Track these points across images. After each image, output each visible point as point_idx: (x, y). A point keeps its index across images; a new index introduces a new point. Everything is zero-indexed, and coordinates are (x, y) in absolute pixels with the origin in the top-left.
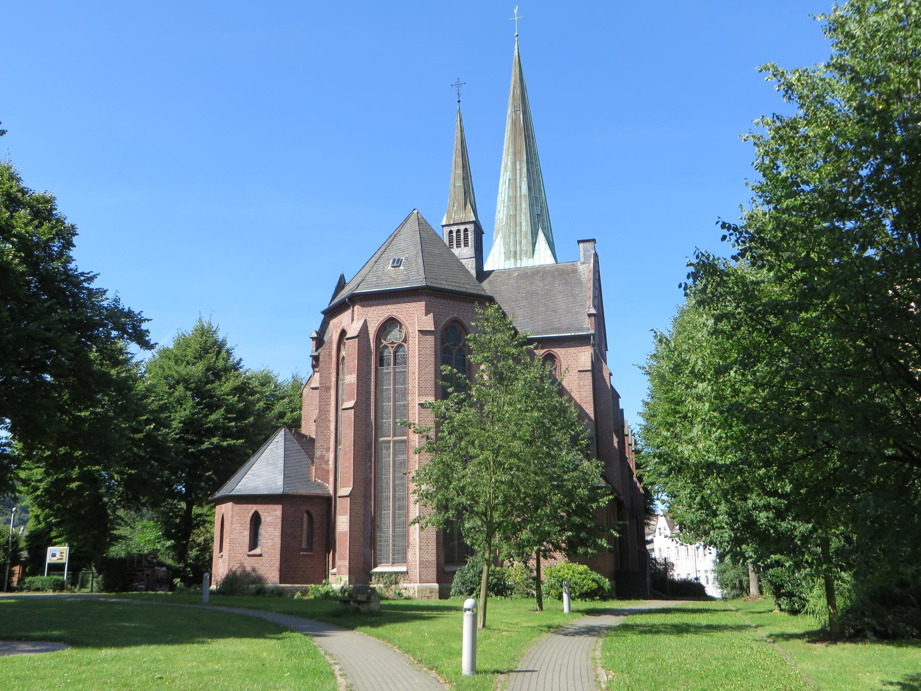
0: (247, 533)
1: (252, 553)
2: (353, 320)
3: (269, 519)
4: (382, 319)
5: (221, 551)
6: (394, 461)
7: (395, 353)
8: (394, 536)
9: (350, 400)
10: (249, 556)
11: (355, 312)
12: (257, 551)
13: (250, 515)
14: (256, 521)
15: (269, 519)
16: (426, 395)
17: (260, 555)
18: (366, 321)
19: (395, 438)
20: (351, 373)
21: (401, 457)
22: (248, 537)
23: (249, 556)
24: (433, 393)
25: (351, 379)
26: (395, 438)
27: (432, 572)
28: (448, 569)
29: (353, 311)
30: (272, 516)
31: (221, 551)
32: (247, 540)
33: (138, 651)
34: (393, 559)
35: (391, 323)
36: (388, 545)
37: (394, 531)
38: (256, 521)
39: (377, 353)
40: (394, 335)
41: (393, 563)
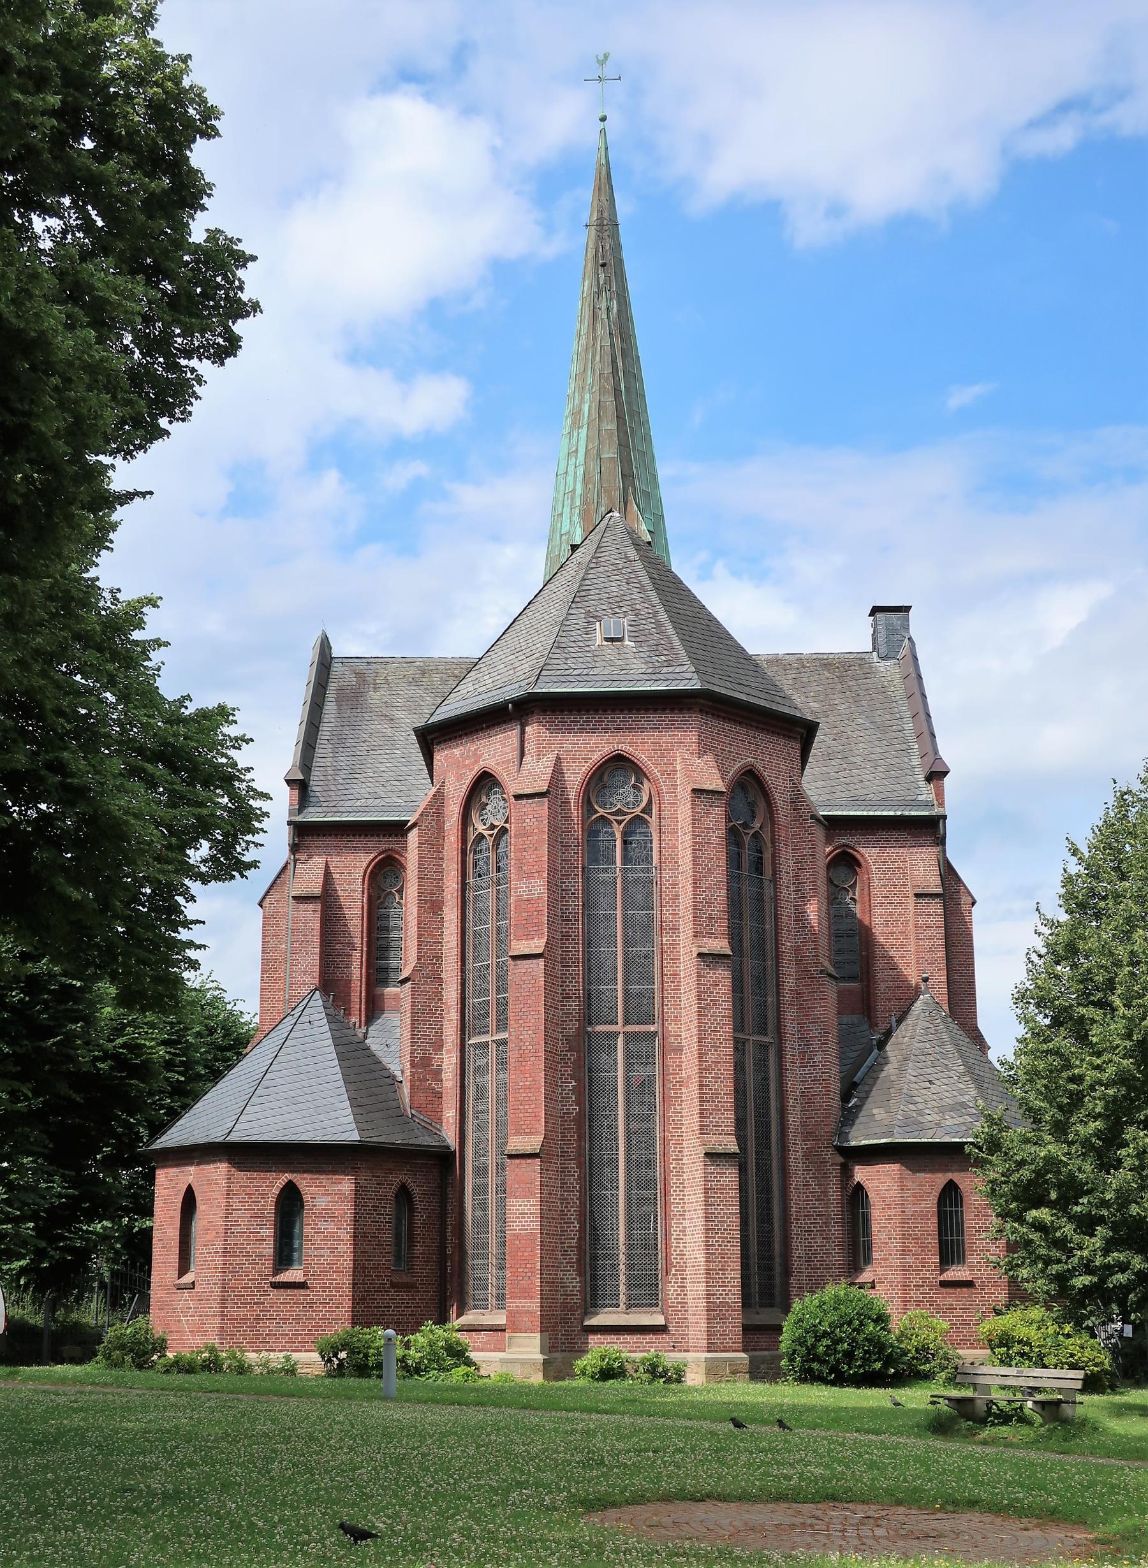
0: (268, 1233)
1: (284, 1277)
2: (522, 754)
3: (322, 1202)
4: (596, 757)
5: (184, 1266)
6: (627, 1079)
7: (625, 834)
8: (630, 1247)
9: (529, 936)
10: (275, 1285)
11: (530, 746)
12: (293, 1275)
13: (276, 1191)
14: (290, 1205)
15: (322, 1202)
16: (711, 935)
17: (302, 1285)
18: (558, 758)
19: (630, 1028)
20: (530, 876)
21: (642, 1072)
22: (271, 1241)
23: (275, 1285)
24: (724, 930)
25: (530, 887)
26: (630, 1028)
27: (733, 1326)
28: (765, 1317)
29: (523, 732)
30: (330, 1199)
31: (184, 1266)
32: (268, 1250)
33: (317, 944)
34: (629, 1298)
35: (619, 765)
36: (615, 1266)
37: (629, 1236)
38: (290, 1205)
39: (600, 820)
40: (624, 798)
41: (629, 1306)
